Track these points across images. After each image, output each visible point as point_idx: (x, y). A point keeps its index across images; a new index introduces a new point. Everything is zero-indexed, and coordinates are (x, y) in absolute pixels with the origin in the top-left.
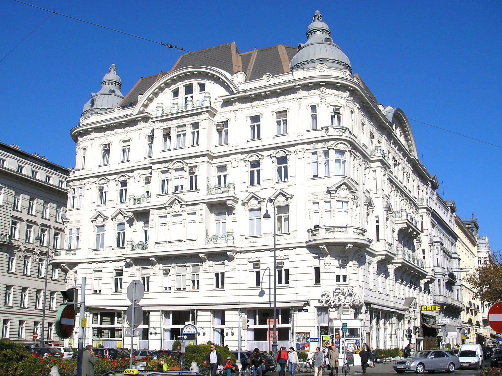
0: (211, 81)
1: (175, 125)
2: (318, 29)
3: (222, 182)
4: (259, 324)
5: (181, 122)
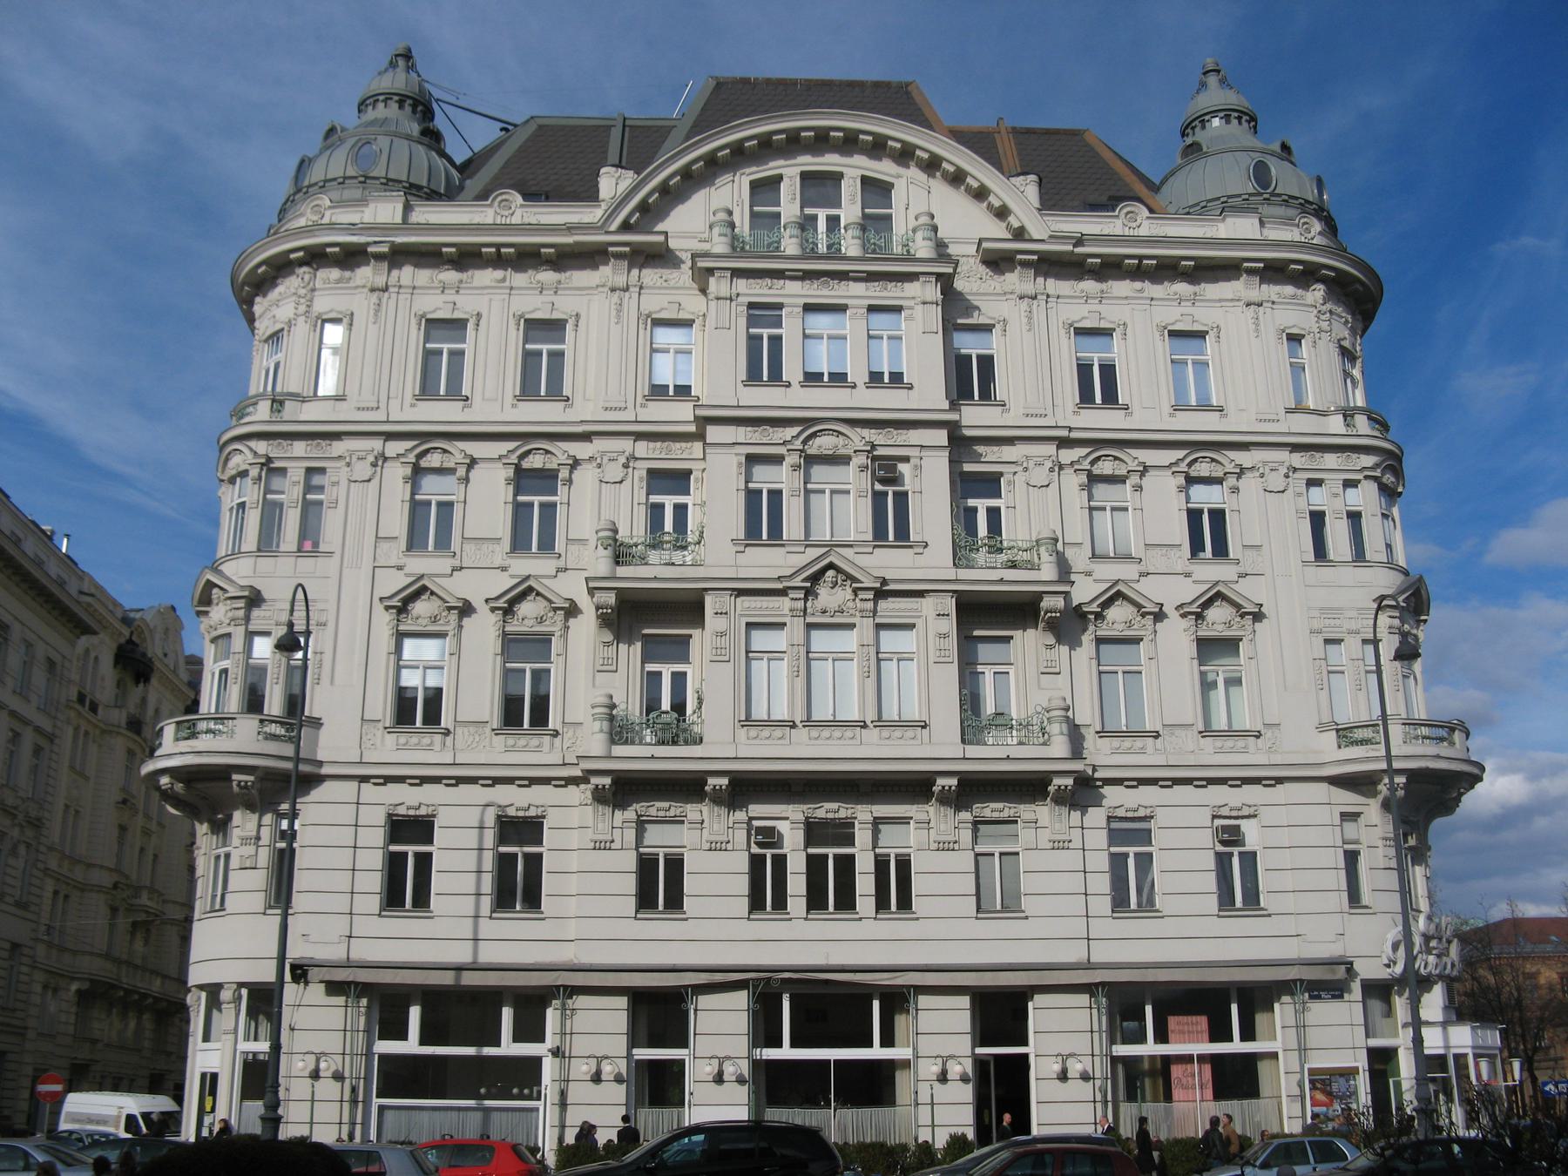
0: (719, 182)
1: (802, 301)
2: (1214, 113)
3: (665, 529)
4: (793, 1045)
5: (825, 292)
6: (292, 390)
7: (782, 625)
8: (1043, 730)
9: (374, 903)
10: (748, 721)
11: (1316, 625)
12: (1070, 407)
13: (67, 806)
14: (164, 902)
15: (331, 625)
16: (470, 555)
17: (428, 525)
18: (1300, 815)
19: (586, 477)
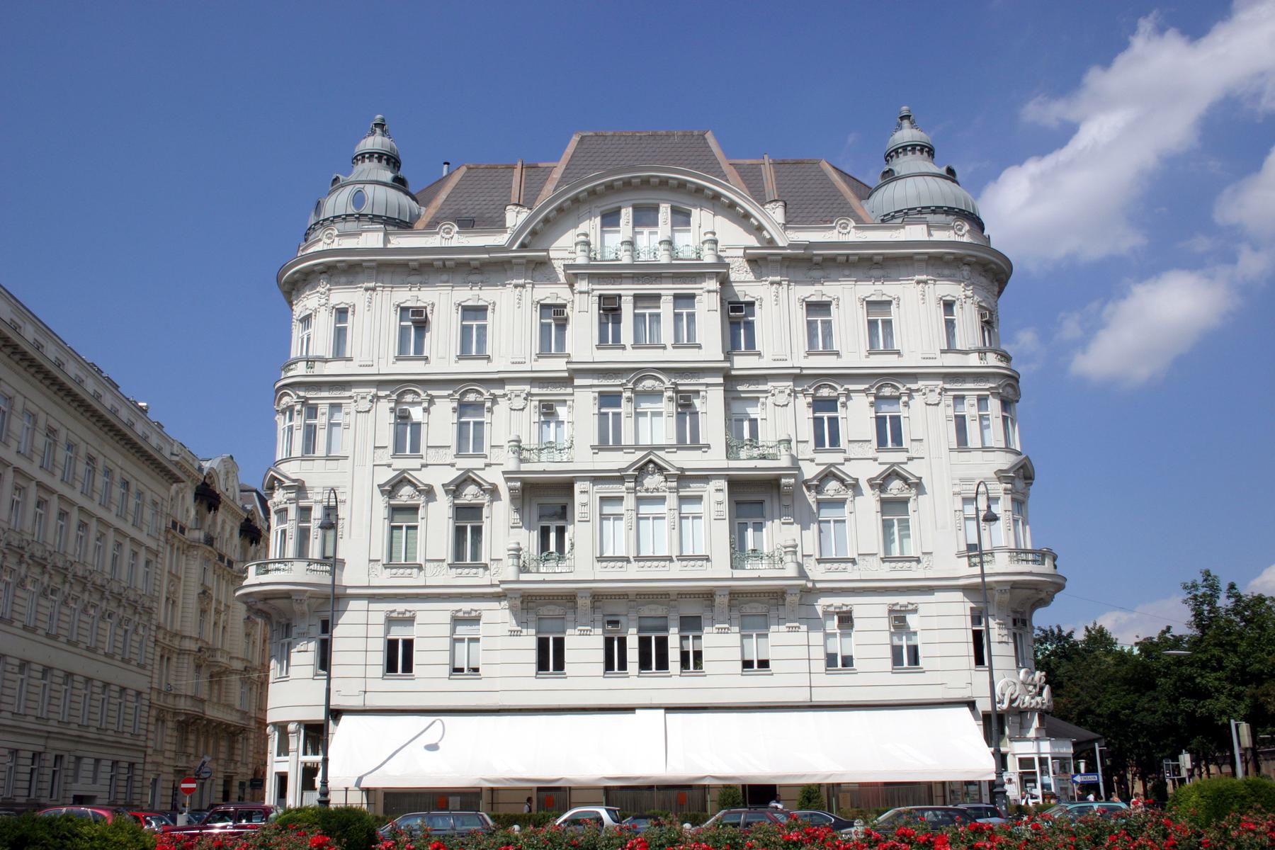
1: (673, 292)
6: (319, 354)
7: (621, 498)
8: (781, 560)
9: (380, 670)
10: (601, 559)
11: (957, 489)
12: (803, 354)
13: (168, 599)
14: (231, 658)
15: (348, 502)
16: (431, 457)
17: (407, 433)
18: (944, 609)
19: (502, 407)
